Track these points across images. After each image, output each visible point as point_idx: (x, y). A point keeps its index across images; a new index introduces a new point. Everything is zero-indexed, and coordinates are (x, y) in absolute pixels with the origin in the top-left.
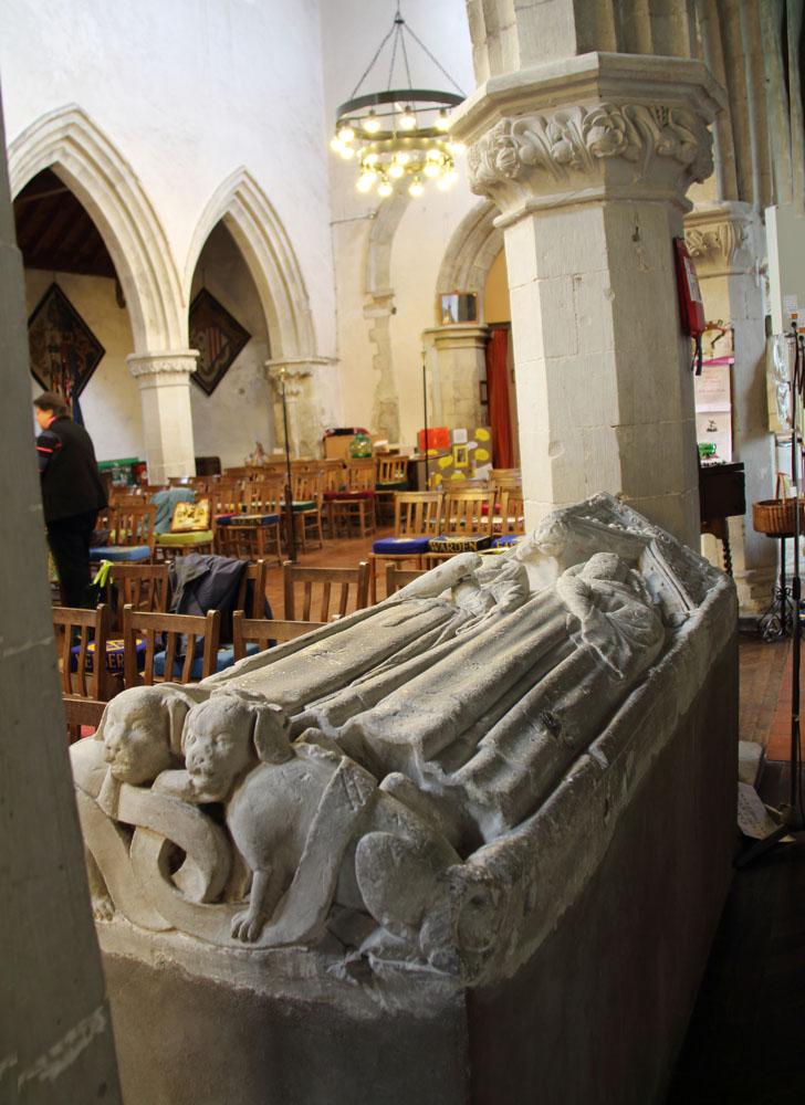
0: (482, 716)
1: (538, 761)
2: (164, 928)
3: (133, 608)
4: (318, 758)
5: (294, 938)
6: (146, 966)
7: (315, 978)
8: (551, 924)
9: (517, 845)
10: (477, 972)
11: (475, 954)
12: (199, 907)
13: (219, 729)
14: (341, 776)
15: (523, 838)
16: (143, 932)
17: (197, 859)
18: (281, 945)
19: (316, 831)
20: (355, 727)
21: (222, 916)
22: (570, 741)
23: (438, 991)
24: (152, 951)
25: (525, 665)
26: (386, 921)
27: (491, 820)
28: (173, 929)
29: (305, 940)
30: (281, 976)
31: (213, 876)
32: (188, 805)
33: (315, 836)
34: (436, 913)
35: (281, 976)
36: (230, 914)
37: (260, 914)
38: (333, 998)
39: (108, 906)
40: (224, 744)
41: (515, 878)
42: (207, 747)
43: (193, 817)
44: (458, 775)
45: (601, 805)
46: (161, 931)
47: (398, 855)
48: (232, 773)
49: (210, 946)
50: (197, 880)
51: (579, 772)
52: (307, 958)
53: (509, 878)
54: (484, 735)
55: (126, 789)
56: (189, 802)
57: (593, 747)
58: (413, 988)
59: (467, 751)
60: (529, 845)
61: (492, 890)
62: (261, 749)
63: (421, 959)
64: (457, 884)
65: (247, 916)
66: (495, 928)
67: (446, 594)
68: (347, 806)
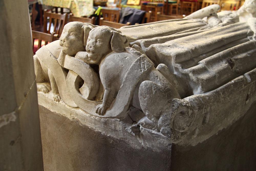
0: (203, 54)
1: (221, 73)
2: (75, 106)
3: (104, 20)
4: (133, 53)
5: (116, 116)
6: (68, 119)
7: (121, 131)
8: (214, 132)
9: (204, 98)
10: (178, 139)
11: (179, 132)
12: (86, 100)
13: (98, 37)
14: (140, 59)
15: (207, 96)
16: (68, 107)
17: (87, 83)
18: (111, 117)
19: (127, 77)
20: (153, 48)
21: (93, 105)
22: (238, 71)
23: (162, 143)
24: (71, 114)
25: (225, 42)
26: (147, 114)
27: (197, 89)
28: (78, 108)
29: (117, 117)
30: (110, 129)
31: (91, 90)
32: (85, 63)
33: (126, 79)
34: (166, 114)
35: (110, 129)
36: (96, 105)
37: (105, 105)
38: (127, 139)
39: (59, 97)
40: (99, 43)
41: (200, 108)
42: (93, 42)
43: (87, 68)
44: (186, 70)
45: (245, 95)
46: (74, 108)
47: (154, 90)
48: (101, 54)
49: (89, 115)
50: (87, 91)
51: (237, 80)
52: (119, 123)
53: (197, 108)
54: (202, 60)
55: (67, 56)
56: (86, 63)
57: (246, 74)
58: (153, 140)
59: (194, 64)
60: (209, 99)
61: (189, 110)
62: (113, 46)
63: (158, 130)
64: (176, 105)
65: (101, 106)
66: (188, 125)
67: (205, 19)
68: (139, 70)
